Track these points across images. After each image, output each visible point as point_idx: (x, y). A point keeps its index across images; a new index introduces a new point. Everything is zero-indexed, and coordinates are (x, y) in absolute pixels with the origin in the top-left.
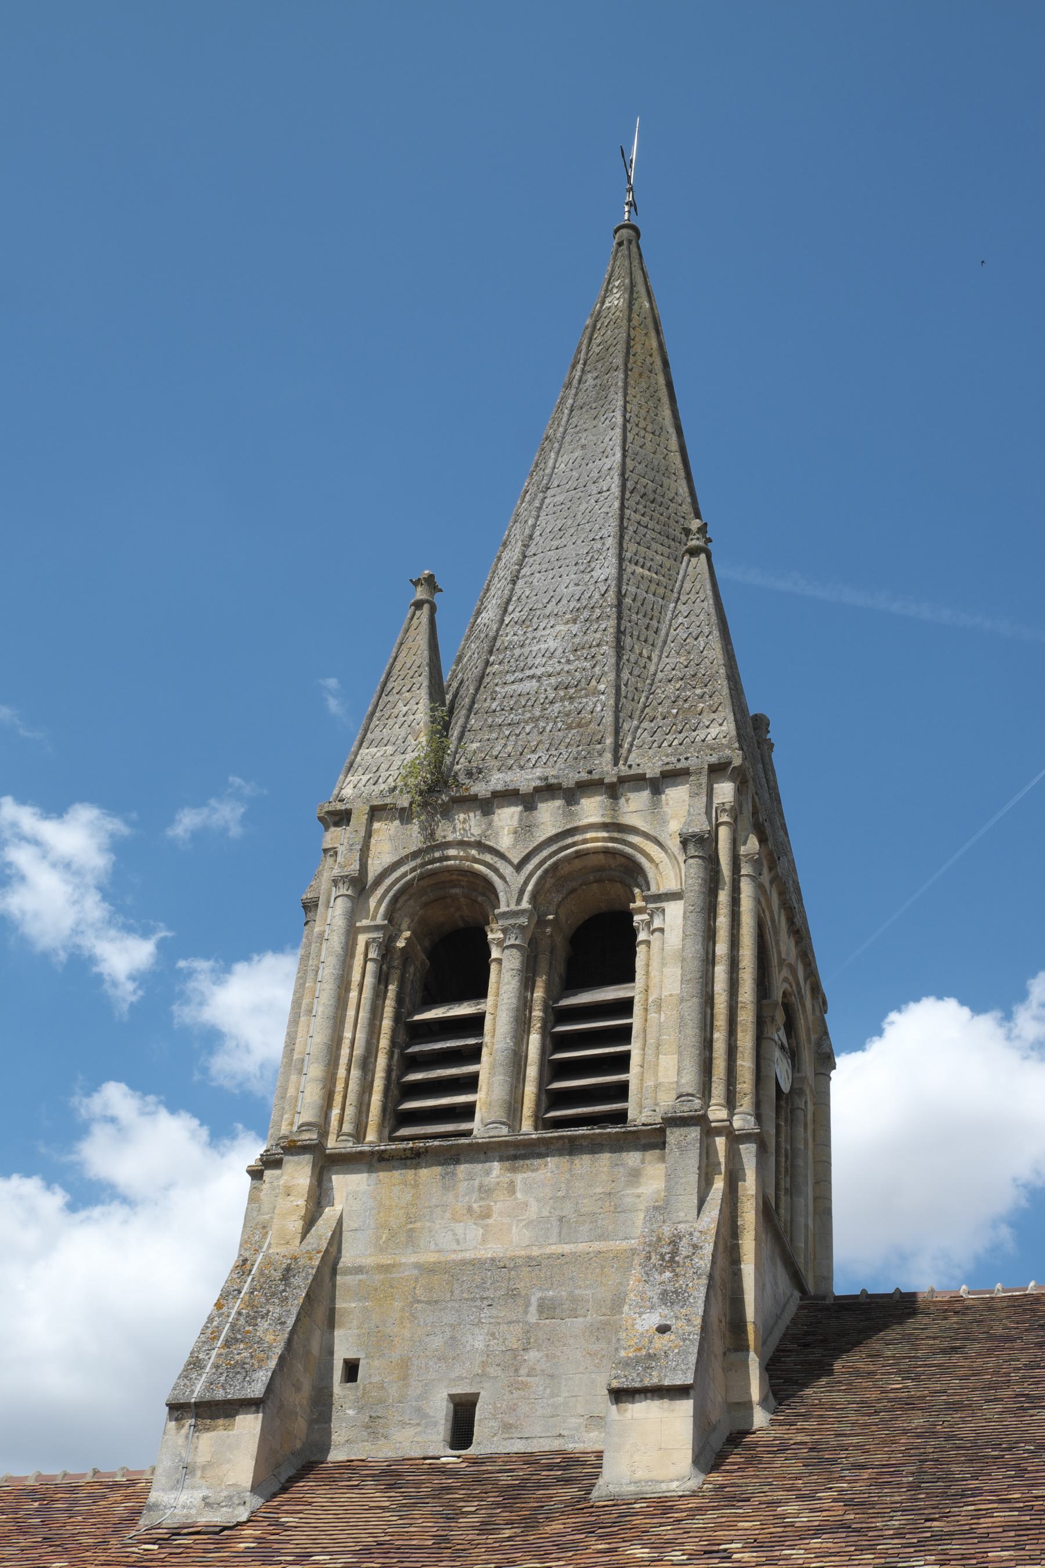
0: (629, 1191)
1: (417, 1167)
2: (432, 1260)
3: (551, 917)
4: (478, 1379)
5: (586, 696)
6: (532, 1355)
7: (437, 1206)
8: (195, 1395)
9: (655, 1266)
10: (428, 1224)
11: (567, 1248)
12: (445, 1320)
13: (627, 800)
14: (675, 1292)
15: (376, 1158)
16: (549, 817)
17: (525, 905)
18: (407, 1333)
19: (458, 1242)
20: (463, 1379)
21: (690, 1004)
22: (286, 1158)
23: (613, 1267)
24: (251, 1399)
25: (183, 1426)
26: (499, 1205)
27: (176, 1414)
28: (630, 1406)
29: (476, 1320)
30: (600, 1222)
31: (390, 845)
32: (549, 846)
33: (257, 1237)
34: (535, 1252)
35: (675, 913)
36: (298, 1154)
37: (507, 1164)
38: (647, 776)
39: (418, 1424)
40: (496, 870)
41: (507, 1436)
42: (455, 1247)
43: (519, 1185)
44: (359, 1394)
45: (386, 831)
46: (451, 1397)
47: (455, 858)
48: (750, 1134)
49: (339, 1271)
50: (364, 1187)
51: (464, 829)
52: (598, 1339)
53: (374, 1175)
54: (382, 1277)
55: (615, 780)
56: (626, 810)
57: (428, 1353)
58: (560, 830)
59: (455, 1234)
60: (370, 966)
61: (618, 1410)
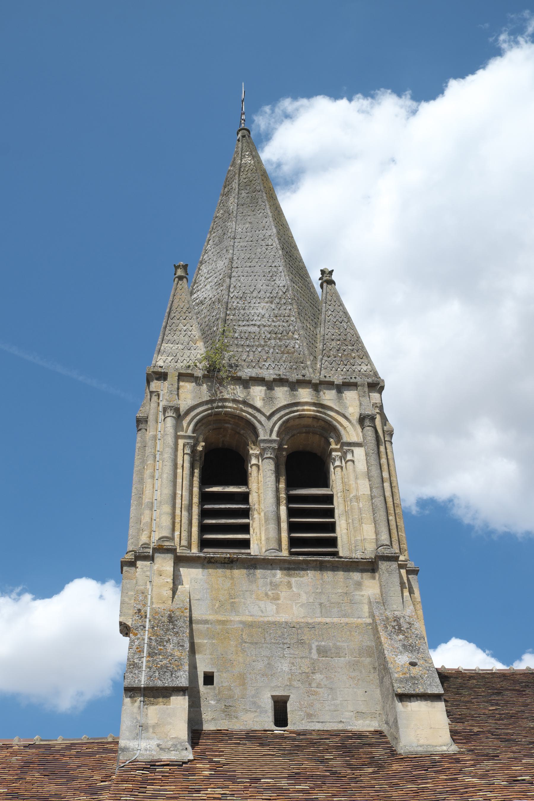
0: (357, 593)
1: (231, 568)
2: (250, 620)
3: (286, 447)
4: (288, 688)
5: (288, 339)
6: (318, 676)
7: (246, 591)
8: (143, 683)
9: (392, 632)
10: (243, 600)
11: (328, 620)
12: (263, 654)
13: (324, 393)
14: (410, 645)
15: (207, 560)
16: (282, 396)
17: (274, 436)
18: (241, 660)
19: (262, 611)
20: (279, 687)
21: (380, 499)
22: (156, 555)
23: (356, 632)
24: (181, 687)
25: (135, 701)
26: (283, 594)
27: (130, 694)
28: (409, 704)
29: (282, 655)
30: (343, 607)
31: (189, 395)
32: (284, 410)
33: (141, 598)
34: (310, 621)
35: (359, 453)
36: (163, 553)
37: (285, 572)
38: (335, 383)
39: (256, 711)
40: (255, 417)
41: (310, 720)
42: (260, 614)
43: (293, 585)
44: (217, 692)
45: (187, 387)
46: (273, 697)
47: (230, 407)
48: (414, 570)
49: (193, 622)
50: (200, 576)
51: (234, 393)
52: (354, 670)
53: (206, 570)
54: (221, 627)
55: (318, 382)
56: (324, 398)
57: (255, 671)
58: (290, 402)
59: (260, 607)
60: (187, 457)
61: (403, 705)
